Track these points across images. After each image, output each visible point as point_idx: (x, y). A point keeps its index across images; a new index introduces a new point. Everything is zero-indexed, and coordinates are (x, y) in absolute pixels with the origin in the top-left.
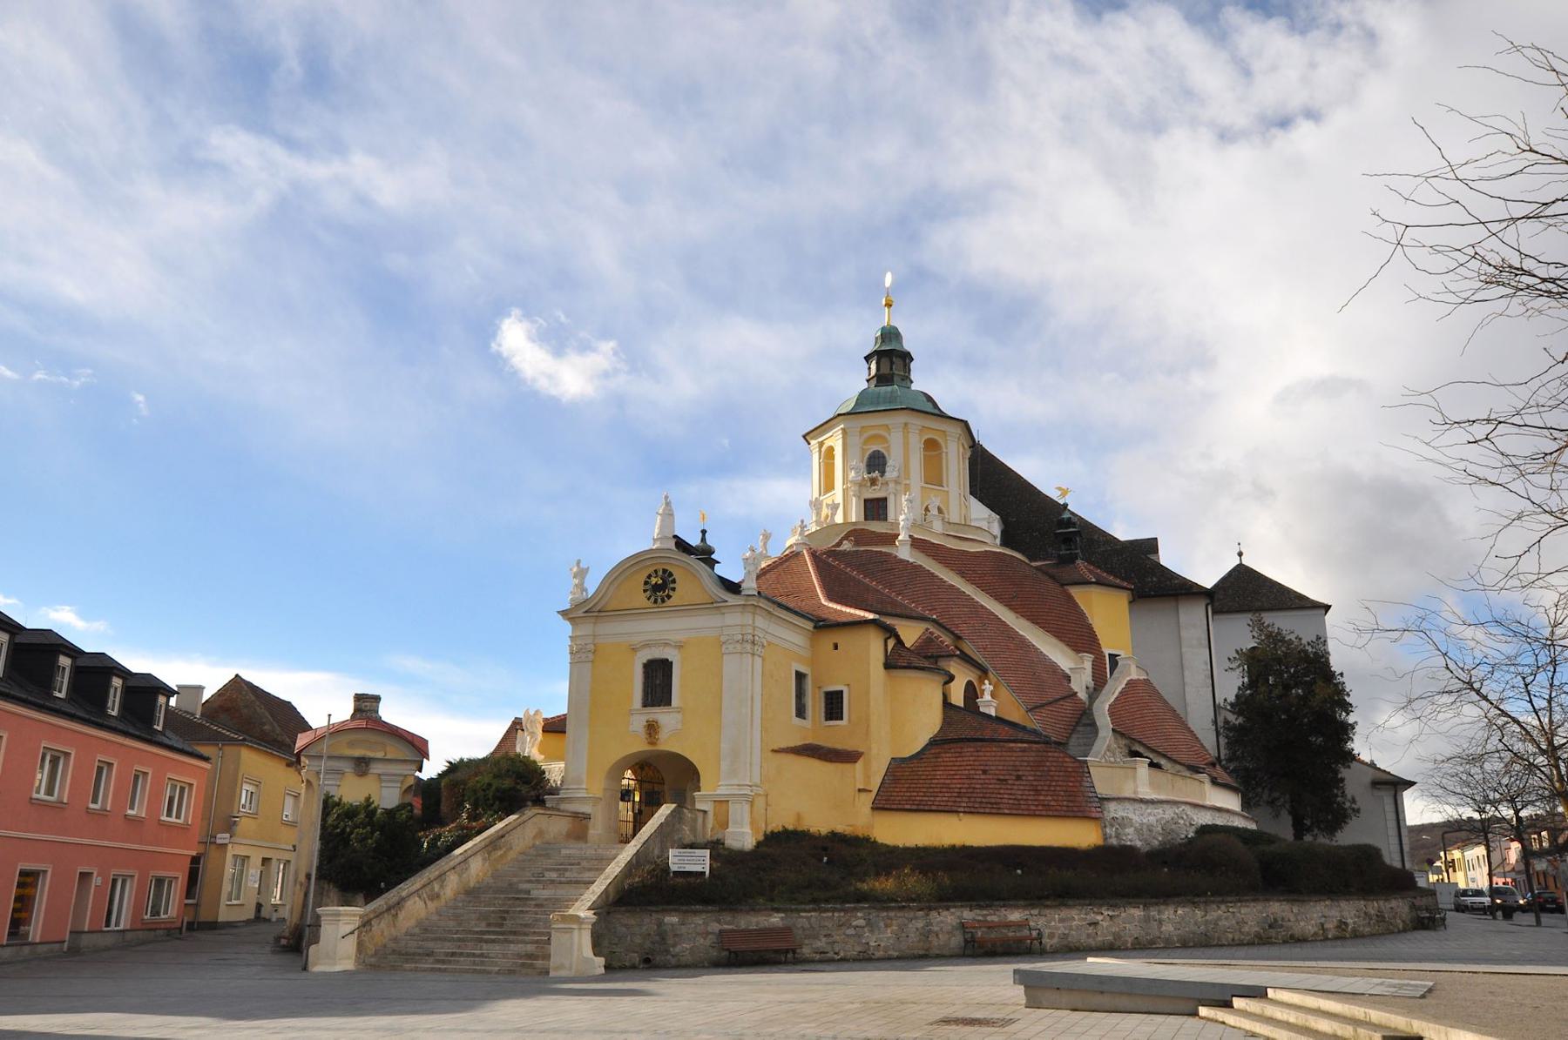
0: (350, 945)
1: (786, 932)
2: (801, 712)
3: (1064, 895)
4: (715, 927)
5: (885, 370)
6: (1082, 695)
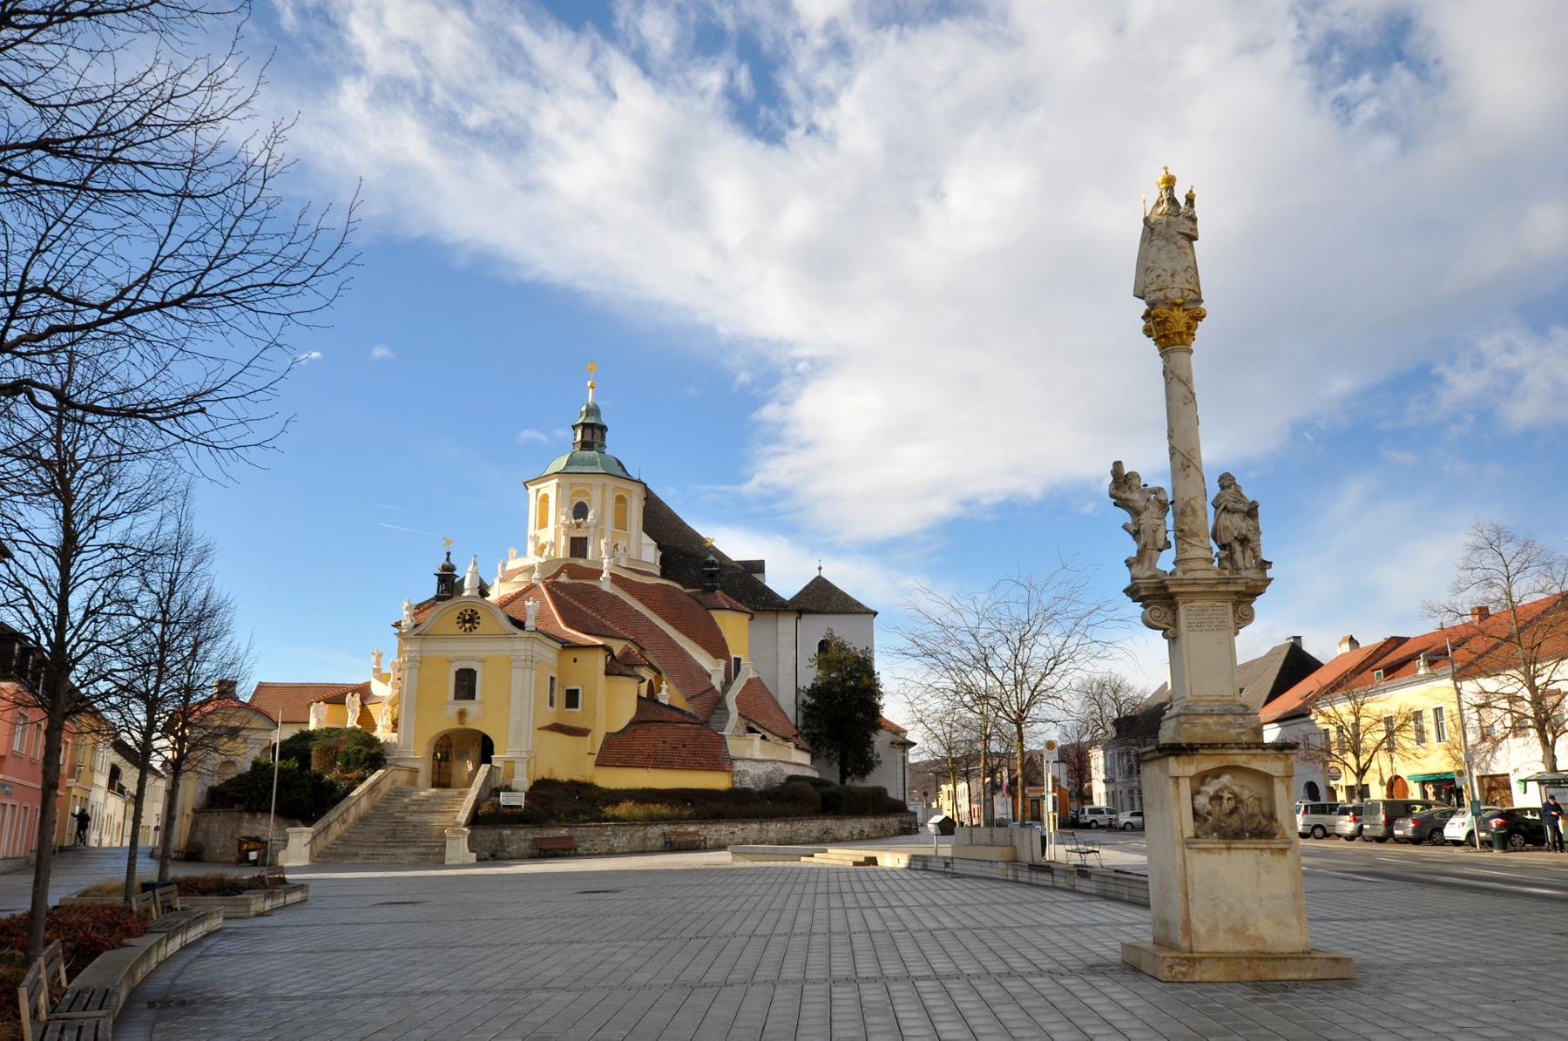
0: (306, 851)
1: (570, 838)
2: (551, 704)
3: (717, 817)
4: (531, 836)
5: (588, 438)
6: (718, 688)
